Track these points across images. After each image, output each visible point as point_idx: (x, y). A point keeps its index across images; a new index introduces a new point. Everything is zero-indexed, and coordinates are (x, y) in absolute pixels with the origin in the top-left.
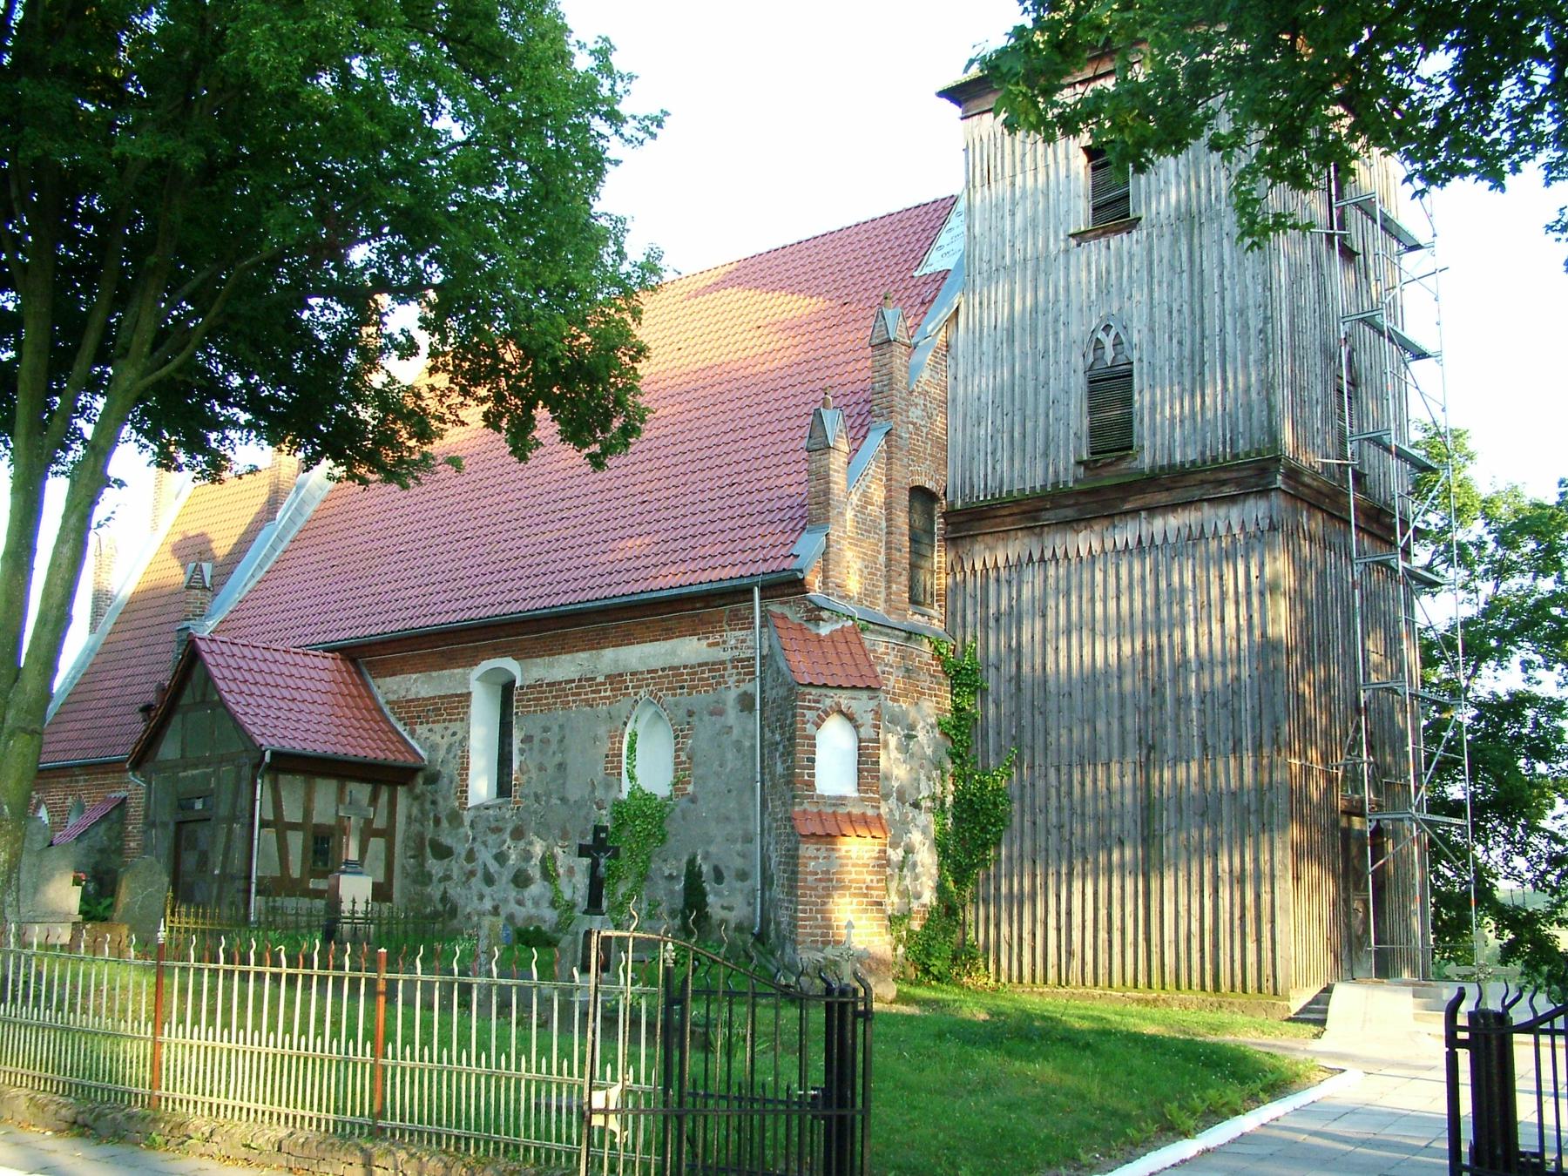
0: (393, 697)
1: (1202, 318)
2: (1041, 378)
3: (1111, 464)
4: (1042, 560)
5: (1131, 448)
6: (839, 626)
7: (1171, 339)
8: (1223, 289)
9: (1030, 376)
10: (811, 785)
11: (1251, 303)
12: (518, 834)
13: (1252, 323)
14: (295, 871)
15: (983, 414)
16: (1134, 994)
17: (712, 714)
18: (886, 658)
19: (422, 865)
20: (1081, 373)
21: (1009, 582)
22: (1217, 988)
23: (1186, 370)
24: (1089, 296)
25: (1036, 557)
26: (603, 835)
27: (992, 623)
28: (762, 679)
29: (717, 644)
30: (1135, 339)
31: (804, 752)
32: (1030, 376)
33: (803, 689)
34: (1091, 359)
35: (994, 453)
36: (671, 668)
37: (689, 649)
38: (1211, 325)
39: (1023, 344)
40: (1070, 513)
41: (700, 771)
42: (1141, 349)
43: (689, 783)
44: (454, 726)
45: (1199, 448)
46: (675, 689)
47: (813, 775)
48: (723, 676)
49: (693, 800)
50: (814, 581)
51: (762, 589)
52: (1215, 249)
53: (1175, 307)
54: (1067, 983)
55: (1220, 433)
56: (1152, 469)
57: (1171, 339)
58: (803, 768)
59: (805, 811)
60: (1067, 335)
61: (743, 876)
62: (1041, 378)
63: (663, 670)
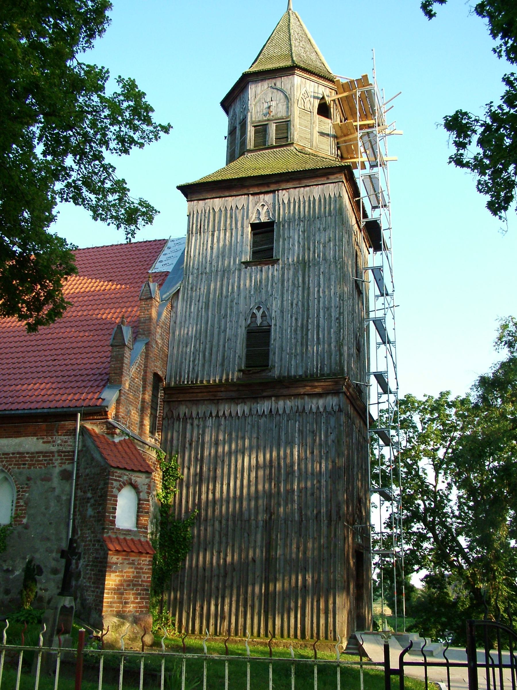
1: (308, 310)
2: (222, 328)
3: (258, 373)
4: (217, 416)
5: (268, 366)
6: (122, 438)
7: (291, 317)
8: (319, 297)
9: (216, 325)
10: (113, 522)
11: (333, 305)
13: (333, 315)
15: (190, 342)
16: (258, 640)
17: (42, 480)
20: (244, 328)
21: (198, 426)
22: (303, 636)
23: (299, 332)
24: (250, 292)
25: (214, 414)
26: (75, 545)
27: (187, 445)
28: (78, 463)
29: (49, 442)
30: (273, 315)
31: (112, 504)
32: (216, 325)
33: (112, 469)
34: (249, 321)
35: (194, 361)
36: (18, 453)
37: (30, 444)
38: (314, 312)
39: (213, 310)
40: (234, 394)
41: (32, 511)
42: (276, 320)
43: (24, 517)
45: (304, 369)
46: (20, 464)
47: (115, 517)
48: (51, 460)
49: (26, 527)
50: (111, 412)
52: (316, 278)
53: (295, 302)
54: (220, 633)
55: (315, 363)
56: (279, 377)
57: (291, 317)
58: (110, 513)
59: (109, 537)
60: (238, 309)
61: (55, 571)
62: (222, 328)
63: (13, 454)
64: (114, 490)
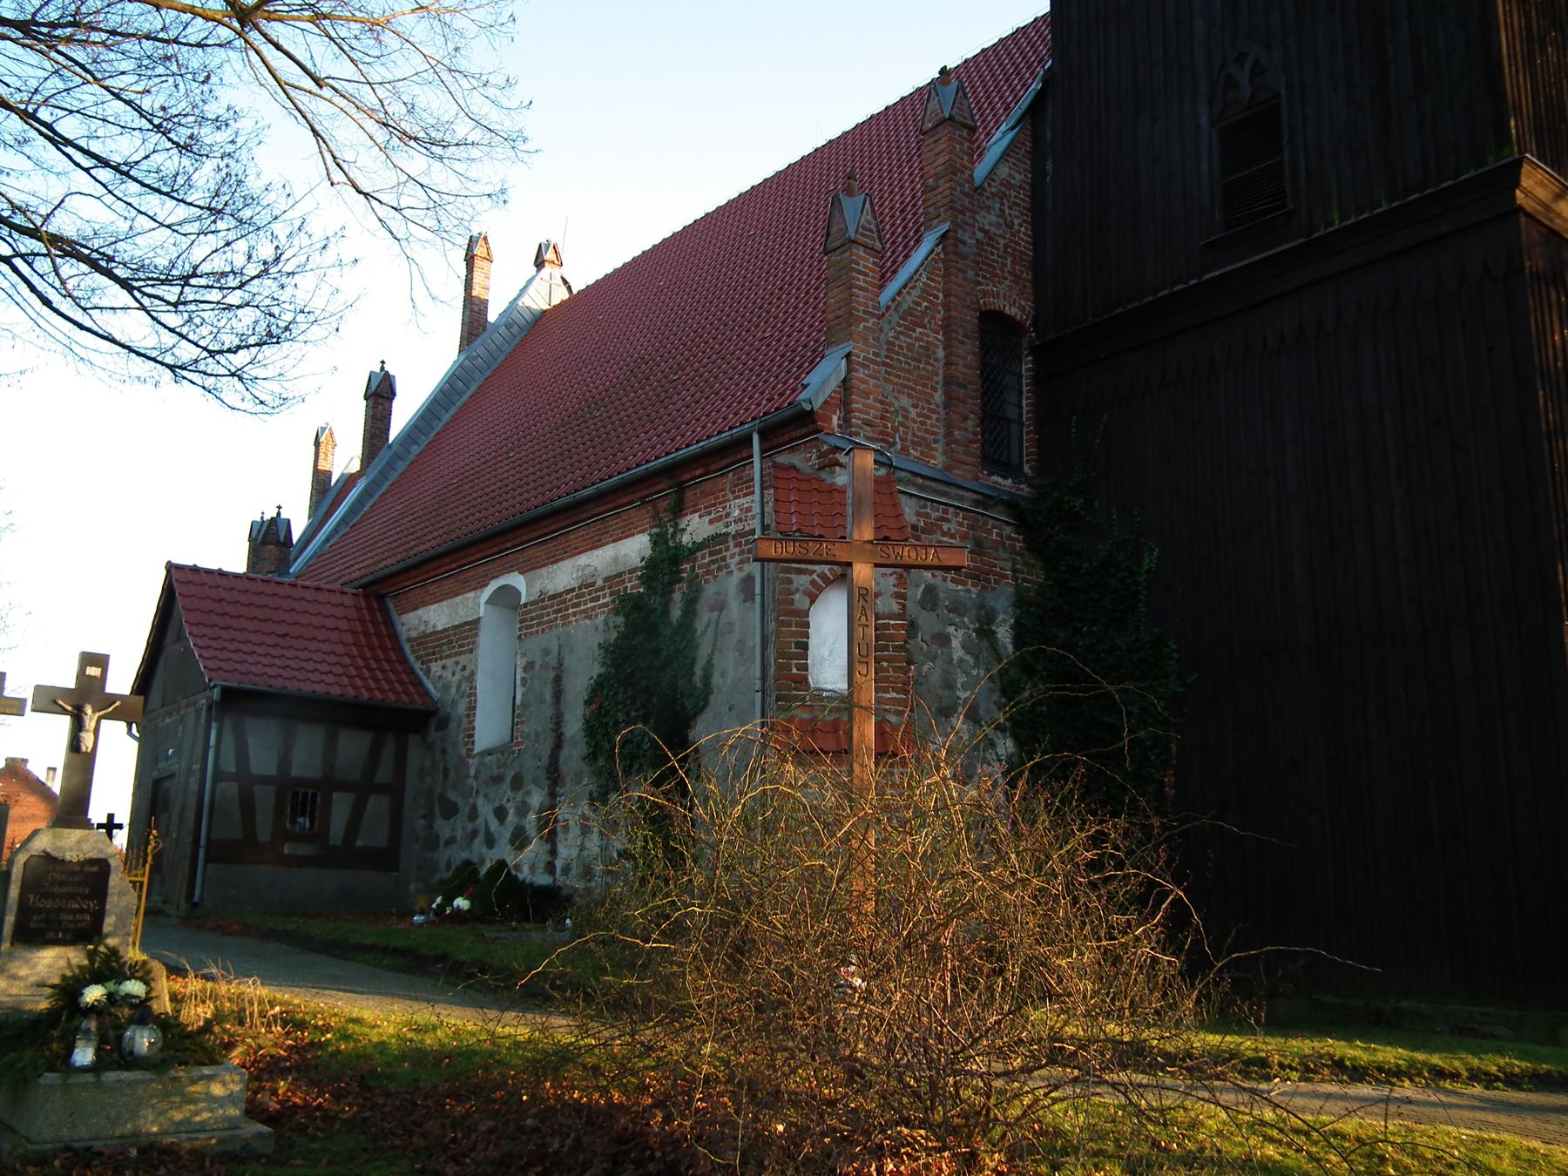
0: (414, 634)
12: (517, 783)
14: (264, 833)
18: (945, 527)
19: (430, 826)
31: (794, 634)
44: (463, 659)
47: (805, 668)
48: (724, 559)
51: (764, 435)
64: (797, 597)
